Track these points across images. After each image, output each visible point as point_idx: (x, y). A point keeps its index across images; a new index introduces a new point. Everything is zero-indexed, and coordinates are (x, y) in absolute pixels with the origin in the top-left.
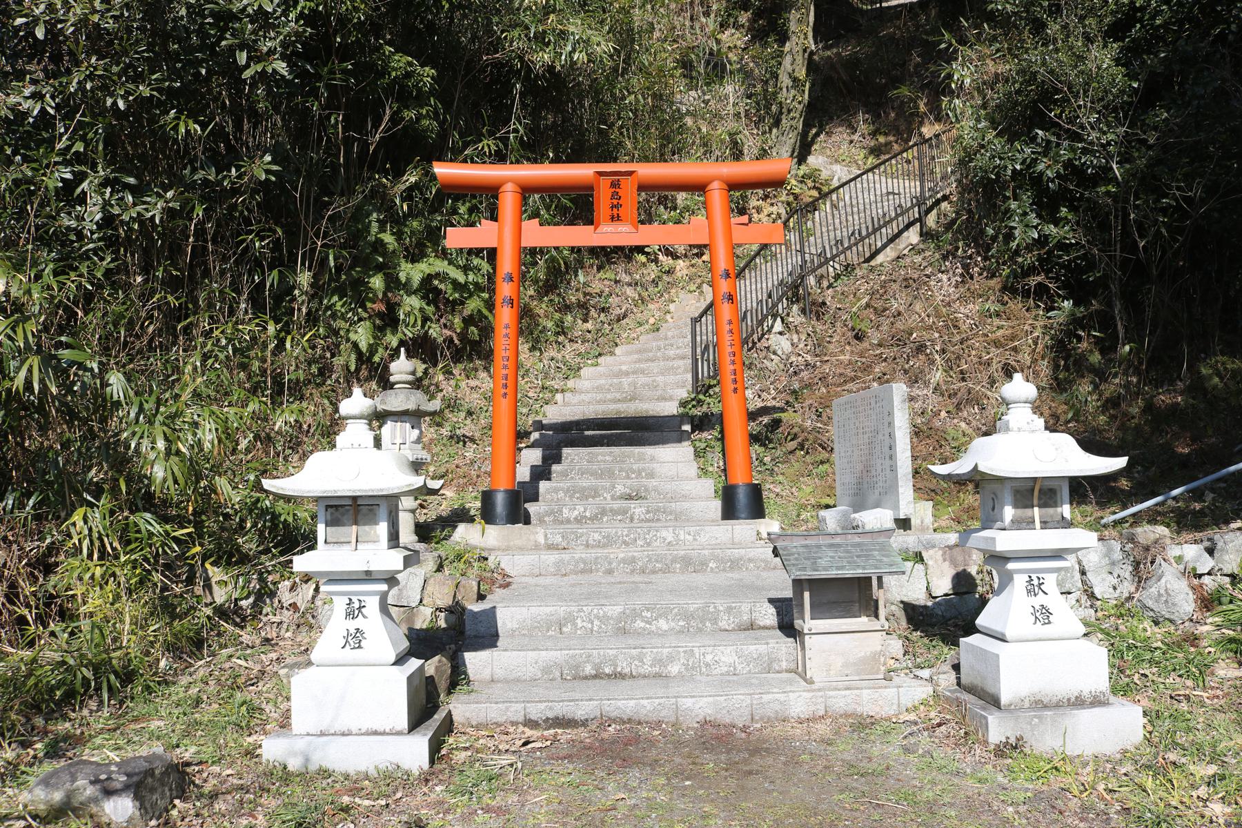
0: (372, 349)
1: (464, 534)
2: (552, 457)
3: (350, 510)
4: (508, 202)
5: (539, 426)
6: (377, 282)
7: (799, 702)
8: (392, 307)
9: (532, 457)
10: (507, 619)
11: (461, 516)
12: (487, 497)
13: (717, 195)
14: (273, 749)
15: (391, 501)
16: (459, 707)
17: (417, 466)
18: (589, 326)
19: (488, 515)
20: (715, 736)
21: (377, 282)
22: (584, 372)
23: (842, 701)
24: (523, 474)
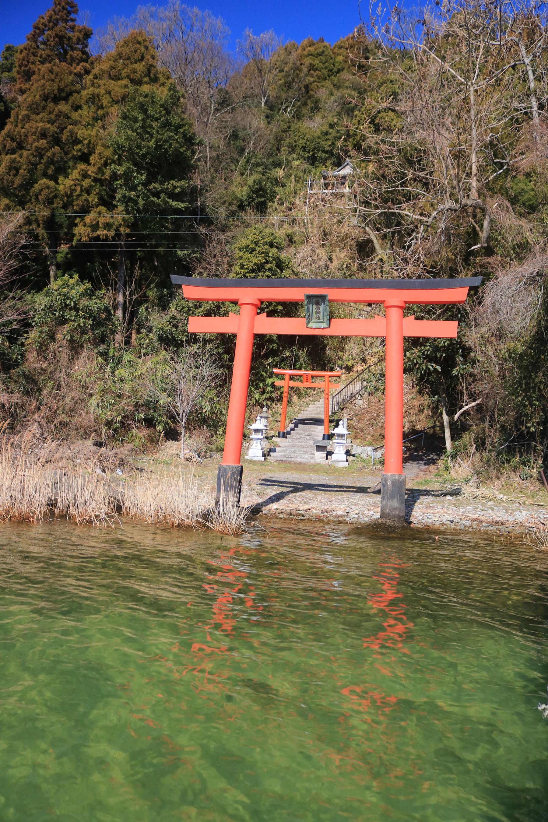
0: (259, 399)
1: (274, 439)
2: (296, 426)
3: (257, 431)
4: (287, 377)
5: (295, 419)
6: (261, 385)
7: (312, 461)
8: (264, 389)
9: (292, 426)
10: (277, 449)
11: (273, 436)
12: (279, 433)
13: (327, 377)
14: (246, 457)
15: (262, 430)
16: (268, 458)
17: (266, 426)
18: (315, 392)
19: (279, 436)
20: (300, 463)
21: (261, 385)
22: (310, 406)
23: (318, 462)
24: (289, 429)
